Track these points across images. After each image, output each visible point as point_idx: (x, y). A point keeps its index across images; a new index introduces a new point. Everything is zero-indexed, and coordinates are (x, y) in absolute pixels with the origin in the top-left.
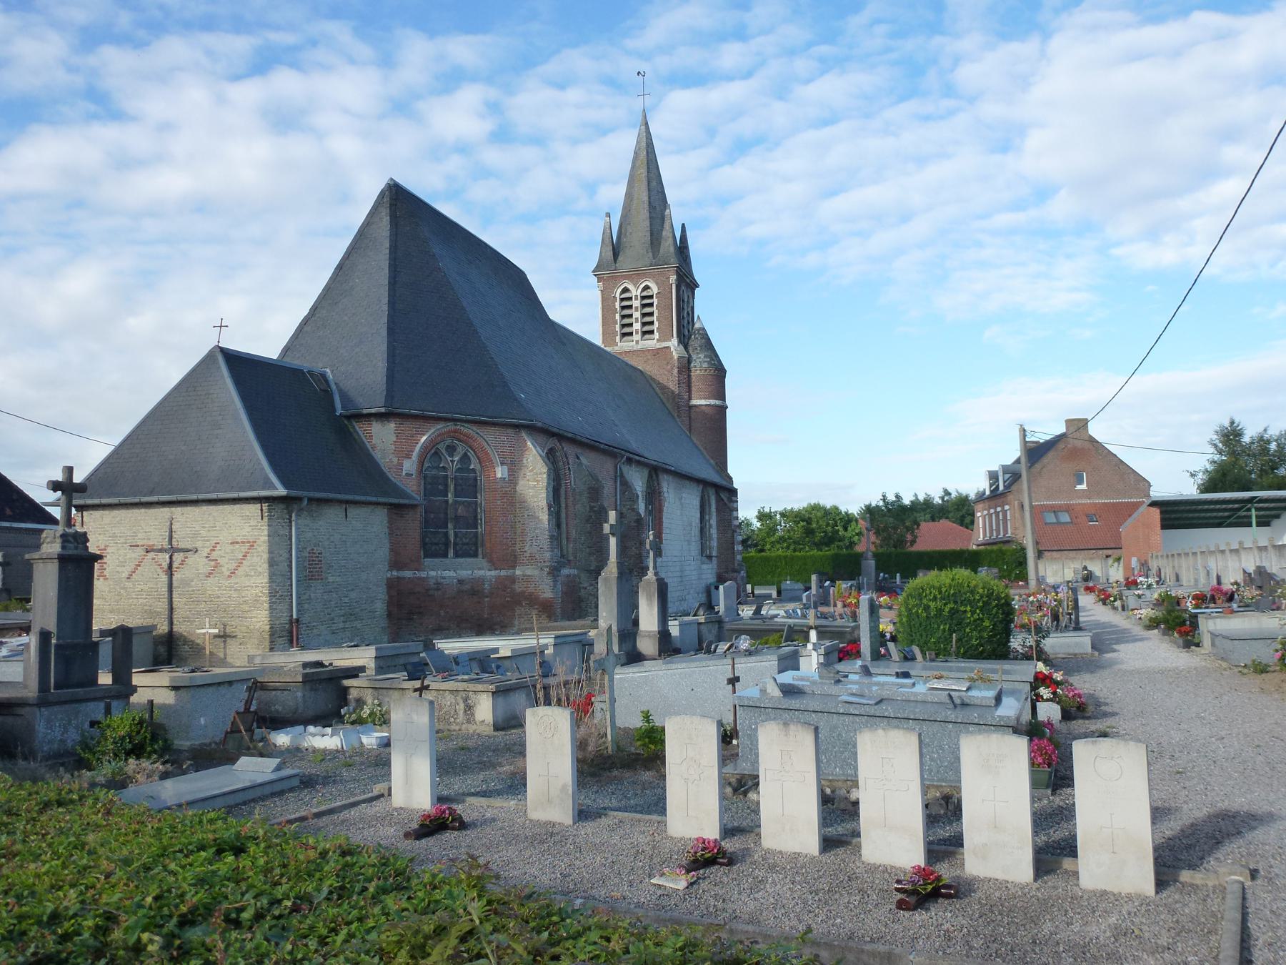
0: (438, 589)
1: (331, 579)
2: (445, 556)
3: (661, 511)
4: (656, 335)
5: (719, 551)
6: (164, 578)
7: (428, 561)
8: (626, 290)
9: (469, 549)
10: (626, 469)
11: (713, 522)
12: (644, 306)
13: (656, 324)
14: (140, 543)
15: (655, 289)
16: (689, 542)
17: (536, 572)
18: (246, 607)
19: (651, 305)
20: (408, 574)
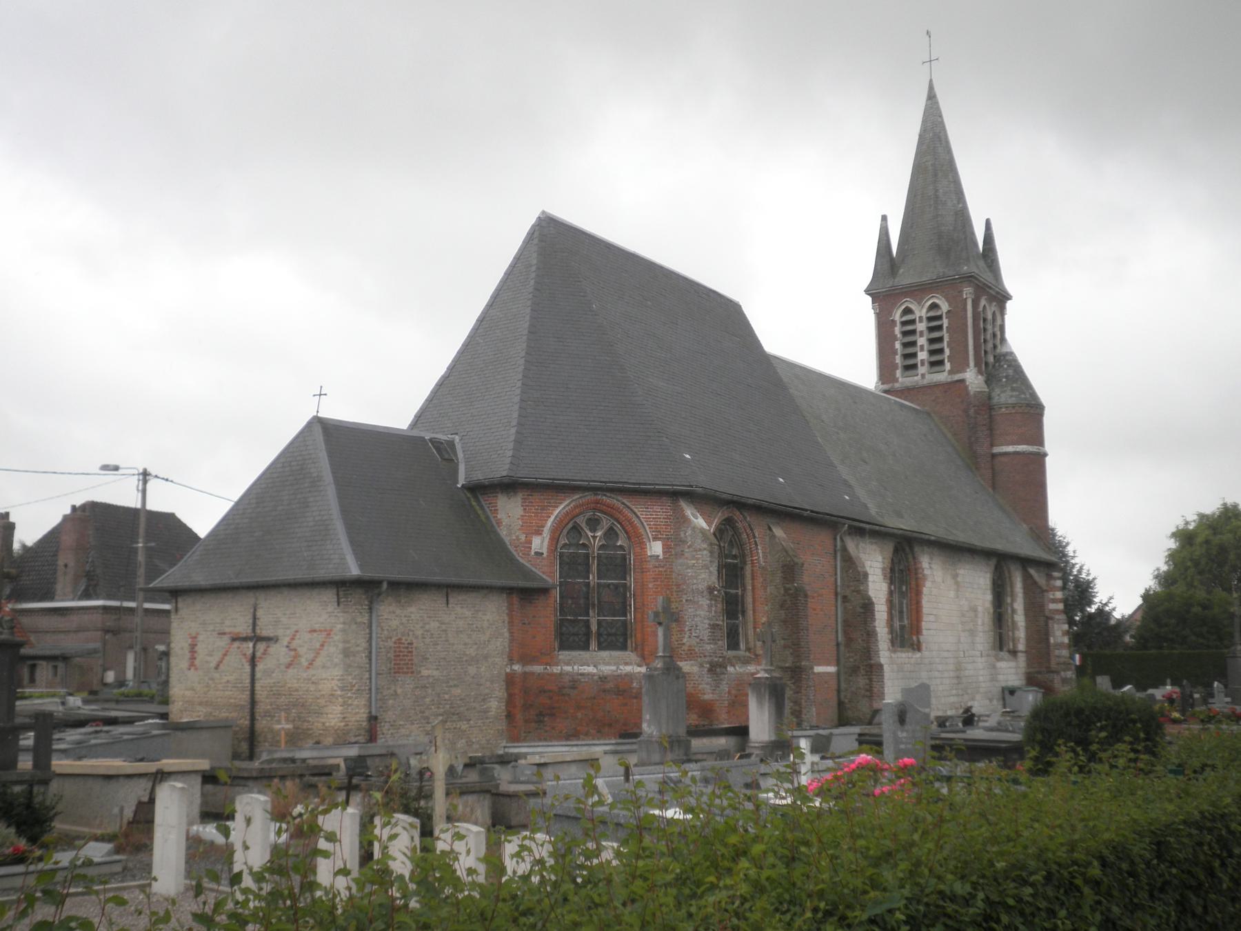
0: (574, 688)
1: (425, 672)
2: (586, 647)
3: (918, 593)
4: (948, 366)
5: (1028, 645)
6: (248, 668)
7: (564, 655)
8: (908, 311)
9: (616, 639)
10: (851, 544)
11: (1019, 605)
12: (931, 329)
13: (947, 352)
14: (227, 630)
15: (945, 307)
16: (972, 633)
17: (695, 669)
18: (322, 702)
19: (940, 328)
20: (538, 669)
